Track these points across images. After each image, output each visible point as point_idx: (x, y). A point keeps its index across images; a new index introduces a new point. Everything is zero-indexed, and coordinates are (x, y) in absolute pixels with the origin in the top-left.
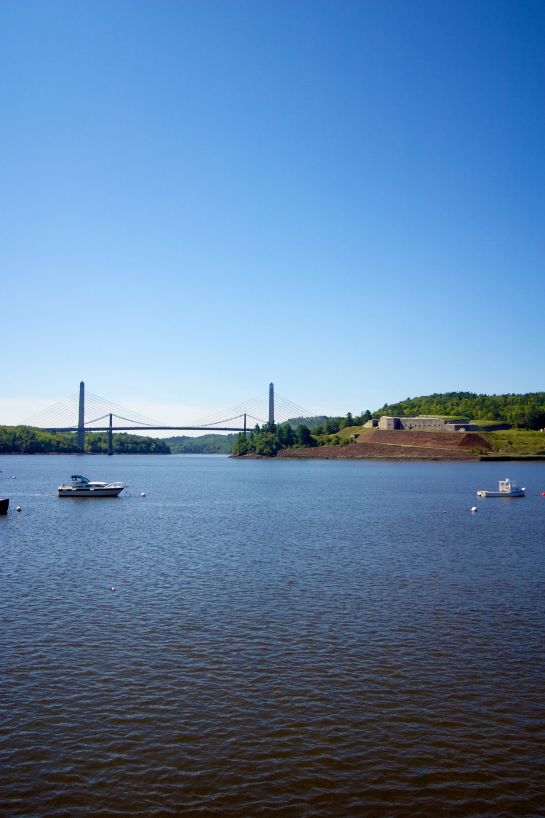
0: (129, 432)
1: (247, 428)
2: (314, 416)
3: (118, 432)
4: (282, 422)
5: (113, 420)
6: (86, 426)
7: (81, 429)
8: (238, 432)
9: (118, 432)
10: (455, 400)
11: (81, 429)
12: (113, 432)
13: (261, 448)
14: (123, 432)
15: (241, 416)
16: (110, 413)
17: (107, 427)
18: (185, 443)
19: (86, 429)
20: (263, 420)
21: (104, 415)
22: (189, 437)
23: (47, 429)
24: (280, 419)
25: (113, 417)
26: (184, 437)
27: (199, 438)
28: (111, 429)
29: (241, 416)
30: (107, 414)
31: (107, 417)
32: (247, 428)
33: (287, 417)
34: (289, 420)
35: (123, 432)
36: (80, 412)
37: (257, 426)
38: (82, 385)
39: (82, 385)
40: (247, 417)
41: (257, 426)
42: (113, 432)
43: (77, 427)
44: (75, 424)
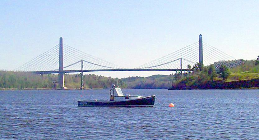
0: (97, 74)
1: (182, 68)
2: (234, 60)
3: (88, 73)
4: (210, 65)
5: (84, 65)
6: (64, 69)
7: (61, 72)
8: (174, 73)
9: (88, 73)
10: (156, 76)
11: (61, 72)
12: (84, 73)
13: (14, 76)
14: (92, 73)
15: (178, 59)
16: (82, 59)
17: (80, 70)
18: (137, 82)
19: (64, 71)
20: (194, 61)
21: (77, 61)
22: (141, 77)
23: (214, 88)
24: (207, 63)
25: (84, 62)
26: (137, 77)
27: (148, 77)
28: (82, 71)
29: (178, 59)
30: (79, 60)
31: (80, 63)
32: (182, 68)
33: (213, 60)
34: (215, 63)
35: (92, 73)
36: (98, 70)
37: (189, 66)
38: (61, 39)
39: (61, 39)
40: (182, 60)
41: (189, 66)
42: (84, 73)
43: (58, 70)
44: (57, 68)
